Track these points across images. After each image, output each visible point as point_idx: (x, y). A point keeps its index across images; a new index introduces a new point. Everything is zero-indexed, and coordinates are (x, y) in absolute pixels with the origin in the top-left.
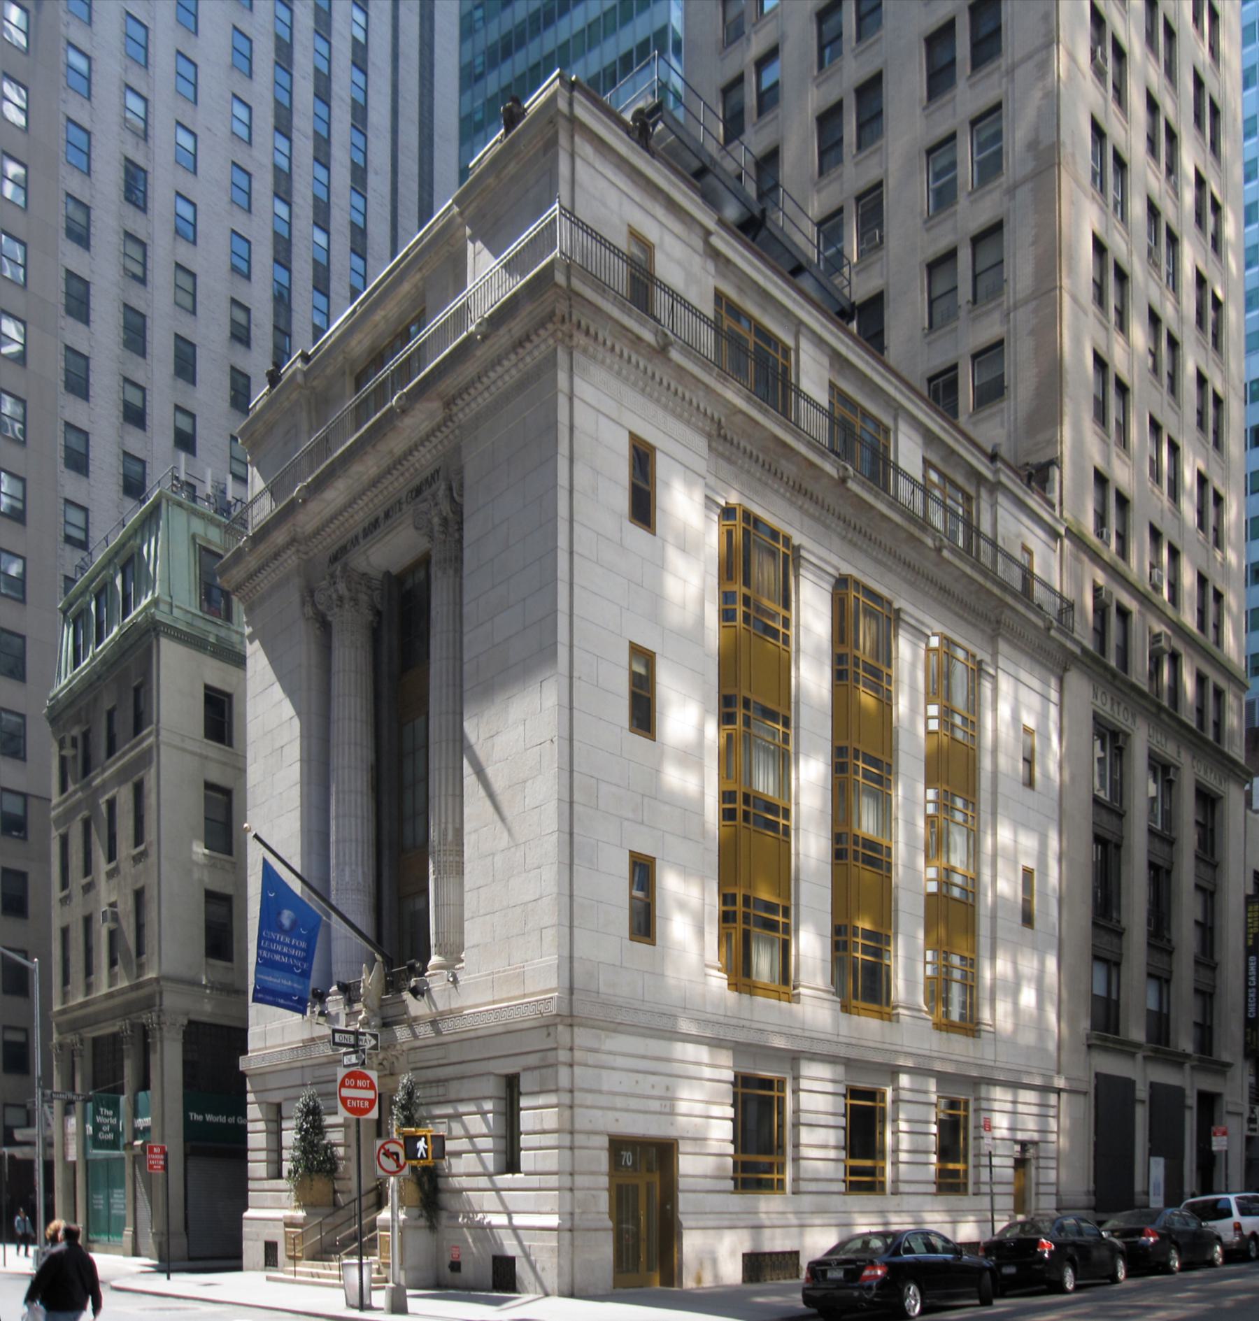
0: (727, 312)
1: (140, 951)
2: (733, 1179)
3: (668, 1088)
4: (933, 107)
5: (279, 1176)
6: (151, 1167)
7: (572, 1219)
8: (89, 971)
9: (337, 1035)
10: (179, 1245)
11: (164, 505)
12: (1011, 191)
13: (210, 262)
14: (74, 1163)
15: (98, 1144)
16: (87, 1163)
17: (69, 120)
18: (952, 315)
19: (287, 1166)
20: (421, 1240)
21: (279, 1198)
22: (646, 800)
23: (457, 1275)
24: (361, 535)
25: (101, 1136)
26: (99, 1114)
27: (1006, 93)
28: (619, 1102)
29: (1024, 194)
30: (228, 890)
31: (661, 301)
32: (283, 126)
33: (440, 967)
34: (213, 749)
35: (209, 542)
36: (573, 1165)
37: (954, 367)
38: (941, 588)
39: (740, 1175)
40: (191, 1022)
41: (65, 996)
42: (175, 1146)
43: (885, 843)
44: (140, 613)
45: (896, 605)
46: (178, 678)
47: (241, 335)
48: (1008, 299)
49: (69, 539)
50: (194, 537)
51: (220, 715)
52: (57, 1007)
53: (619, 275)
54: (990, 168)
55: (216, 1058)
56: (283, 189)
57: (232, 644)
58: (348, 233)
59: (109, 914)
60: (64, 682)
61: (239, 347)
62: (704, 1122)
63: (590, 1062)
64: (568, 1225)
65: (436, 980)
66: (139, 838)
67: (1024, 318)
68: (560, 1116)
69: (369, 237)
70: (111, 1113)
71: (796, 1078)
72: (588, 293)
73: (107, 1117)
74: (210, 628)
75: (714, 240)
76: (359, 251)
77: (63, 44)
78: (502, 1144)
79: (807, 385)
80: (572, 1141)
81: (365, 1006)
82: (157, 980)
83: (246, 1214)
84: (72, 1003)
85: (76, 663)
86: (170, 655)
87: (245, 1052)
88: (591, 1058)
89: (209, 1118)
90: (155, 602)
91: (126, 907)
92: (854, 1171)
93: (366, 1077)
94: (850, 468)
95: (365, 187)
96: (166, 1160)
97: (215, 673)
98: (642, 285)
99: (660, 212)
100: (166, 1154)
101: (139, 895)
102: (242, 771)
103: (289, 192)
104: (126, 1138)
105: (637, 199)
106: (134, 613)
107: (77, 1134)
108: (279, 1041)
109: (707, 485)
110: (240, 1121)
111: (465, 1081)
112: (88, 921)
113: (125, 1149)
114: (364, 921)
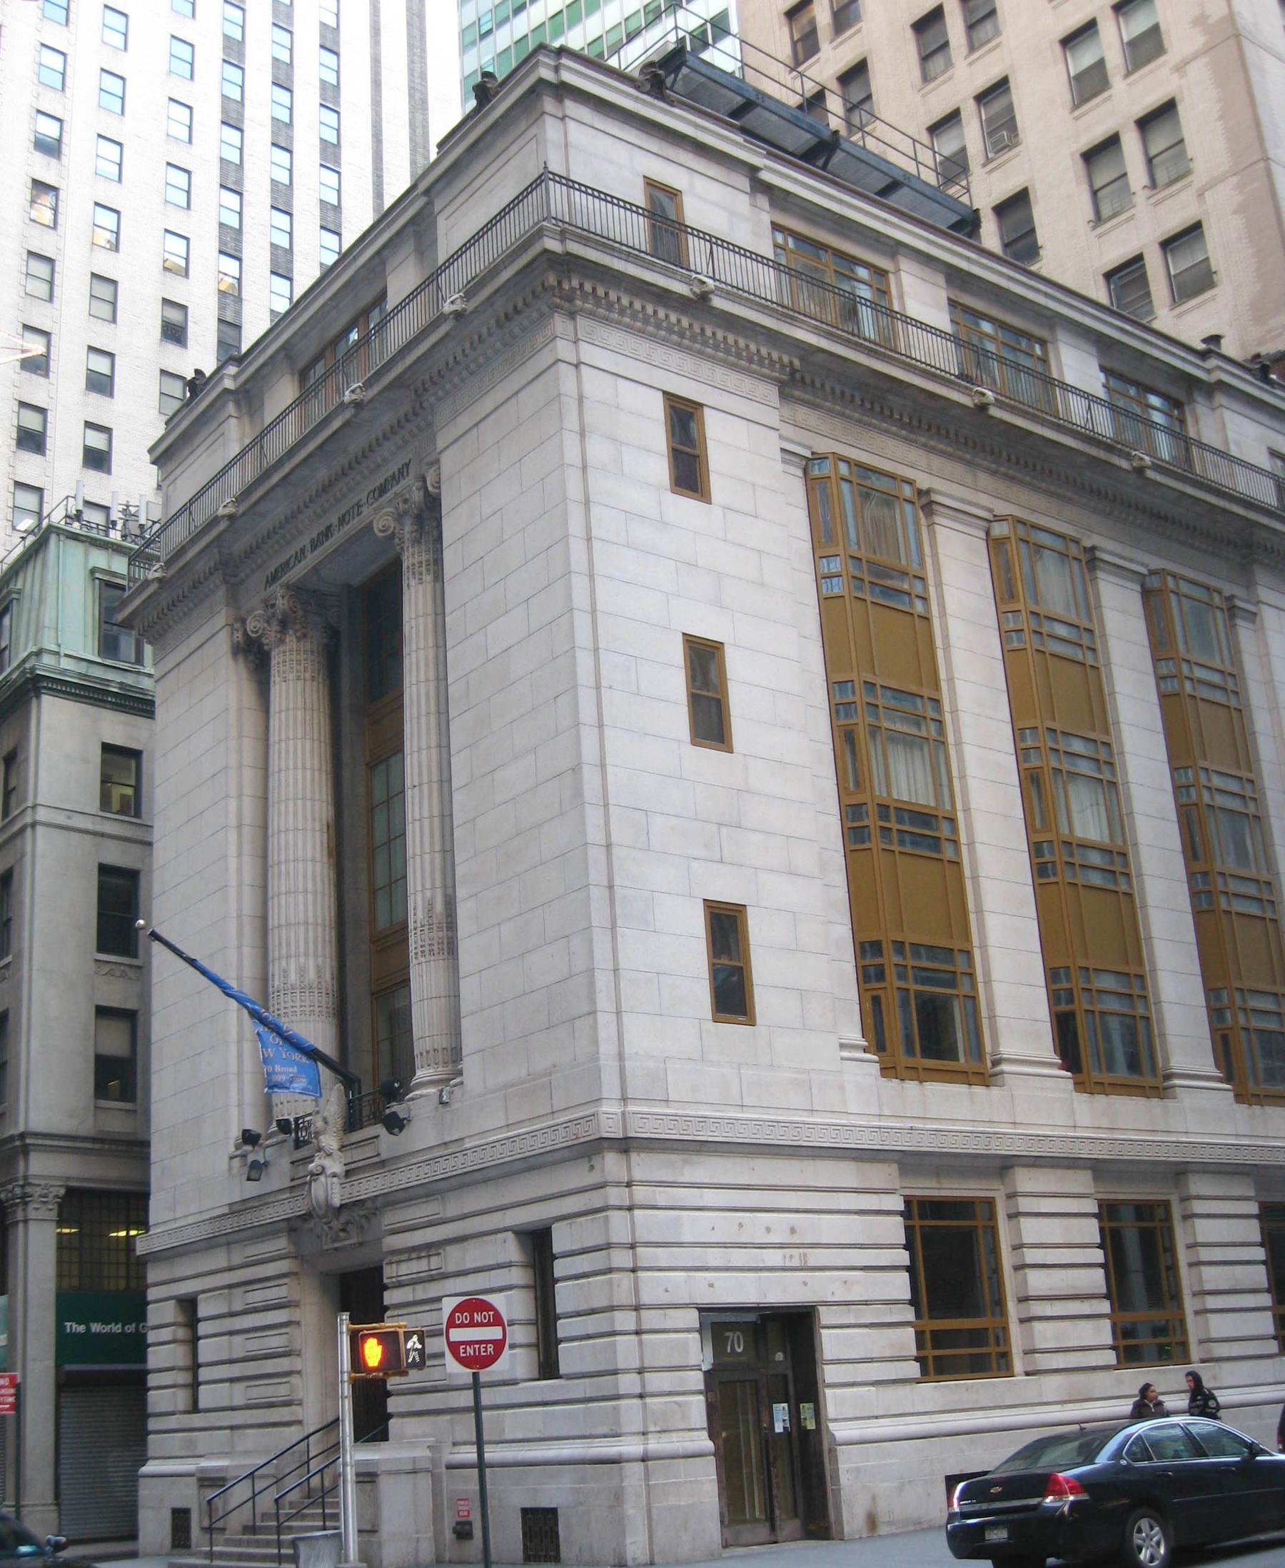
2: (917, 1359)
3: (793, 1231)
12: (1181, 68)
21: (192, 1443)
22: (724, 830)
24: (308, 547)
31: (696, 251)
37: (1139, 258)
38: (1152, 515)
39: (930, 1353)
45: (1088, 543)
53: (636, 231)
58: (317, 212)
61: (172, 348)
62: (853, 1273)
63: (661, 1203)
74: (111, 675)
75: (765, 176)
76: (332, 227)
79: (915, 309)
83: (145, 1469)
89: (96, 1327)
92: (939, 1338)
94: (989, 393)
96: (18, 1396)
97: (117, 728)
108: (193, 1209)
109: (781, 437)
111: (472, 1243)
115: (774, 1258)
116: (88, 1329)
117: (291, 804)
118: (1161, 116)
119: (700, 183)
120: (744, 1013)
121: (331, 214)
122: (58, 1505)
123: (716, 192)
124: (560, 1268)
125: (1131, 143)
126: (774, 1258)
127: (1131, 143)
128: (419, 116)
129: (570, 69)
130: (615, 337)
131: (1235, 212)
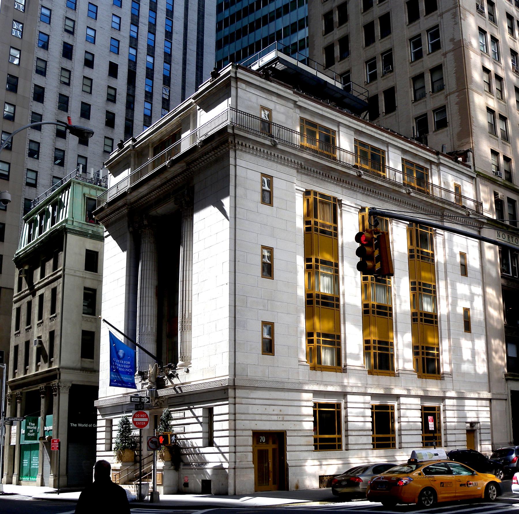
0: (306, 124)
1: (52, 355)
2: (314, 445)
3: (281, 411)
4: (410, 25)
5: (111, 450)
6: (53, 448)
7: (235, 464)
8: (27, 363)
9: (132, 399)
10: (63, 481)
11: (72, 184)
12: (445, 55)
13: (100, 73)
14: (15, 446)
15: (27, 438)
16: (21, 446)
17: (40, 32)
18: (424, 95)
19: (114, 446)
20: (171, 475)
23: (187, 488)
25: (29, 434)
26: (28, 425)
27: (440, 22)
28: (257, 417)
29: (450, 56)
30: (93, 330)
31: (275, 130)
32: (135, 21)
33: (182, 366)
34: (89, 274)
35: (91, 195)
36: (235, 443)
40: (73, 385)
41: (14, 374)
42: (63, 438)
43: (389, 305)
44: (59, 224)
46: (75, 247)
47: (112, 99)
48: (447, 90)
49: (28, 184)
50: (84, 195)
51: (93, 262)
52: (10, 379)
54: (436, 47)
55: (84, 398)
56: (134, 42)
57: (99, 233)
58: (163, 56)
59: (37, 342)
60: (22, 248)
64: (233, 467)
65: (180, 372)
66: (53, 310)
67: (453, 99)
68: (230, 424)
69: (173, 56)
70: (34, 424)
71: (346, 403)
72: (242, 133)
73: (32, 426)
76: (168, 61)
77: (40, 7)
78: (207, 435)
80: (235, 433)
81: (150, 381)
82: (58, 369)
84: (17, 378)
85: (29, 241)
86: (71, 240)
87: (97, 398)
88: (244, 401)
89: (80, 425)
90: (66, 221)
91: (46, 339)
92: (378, 439)
93: (145, 413)
95: (171, 39)
96: (59, 445)
97: (91, 244)
98: (267, 126)
99: (274, 99)
100: (59, 443)
101: (52, 334)
102: (100, 282)
103: (136, 45)
104: (40, 435)
105: (264, 97)
106: (56, 224)
107: (17, 433)
110: (94, 426)
112: (27, 344)
113: (40, 439)
114: (151, 348)
115: (275, 418)
116: (78, 425)
117: (147, 314)
118: (437, 69)
119: (278, 107)
120: (271, 352)
121: (168, 57)
122: (67, 476)
123: (282, 109)
124: (215, 418)
125: (428, 78)
126: (275, 418)
127: (428, 78)
128: (201, 21)
129: (240, 73)
130: (248, 157)
131: (456, 104)
